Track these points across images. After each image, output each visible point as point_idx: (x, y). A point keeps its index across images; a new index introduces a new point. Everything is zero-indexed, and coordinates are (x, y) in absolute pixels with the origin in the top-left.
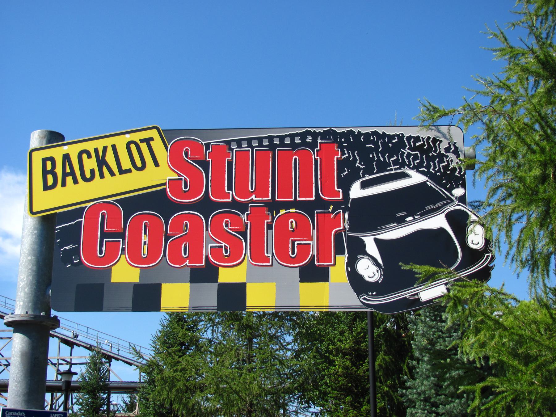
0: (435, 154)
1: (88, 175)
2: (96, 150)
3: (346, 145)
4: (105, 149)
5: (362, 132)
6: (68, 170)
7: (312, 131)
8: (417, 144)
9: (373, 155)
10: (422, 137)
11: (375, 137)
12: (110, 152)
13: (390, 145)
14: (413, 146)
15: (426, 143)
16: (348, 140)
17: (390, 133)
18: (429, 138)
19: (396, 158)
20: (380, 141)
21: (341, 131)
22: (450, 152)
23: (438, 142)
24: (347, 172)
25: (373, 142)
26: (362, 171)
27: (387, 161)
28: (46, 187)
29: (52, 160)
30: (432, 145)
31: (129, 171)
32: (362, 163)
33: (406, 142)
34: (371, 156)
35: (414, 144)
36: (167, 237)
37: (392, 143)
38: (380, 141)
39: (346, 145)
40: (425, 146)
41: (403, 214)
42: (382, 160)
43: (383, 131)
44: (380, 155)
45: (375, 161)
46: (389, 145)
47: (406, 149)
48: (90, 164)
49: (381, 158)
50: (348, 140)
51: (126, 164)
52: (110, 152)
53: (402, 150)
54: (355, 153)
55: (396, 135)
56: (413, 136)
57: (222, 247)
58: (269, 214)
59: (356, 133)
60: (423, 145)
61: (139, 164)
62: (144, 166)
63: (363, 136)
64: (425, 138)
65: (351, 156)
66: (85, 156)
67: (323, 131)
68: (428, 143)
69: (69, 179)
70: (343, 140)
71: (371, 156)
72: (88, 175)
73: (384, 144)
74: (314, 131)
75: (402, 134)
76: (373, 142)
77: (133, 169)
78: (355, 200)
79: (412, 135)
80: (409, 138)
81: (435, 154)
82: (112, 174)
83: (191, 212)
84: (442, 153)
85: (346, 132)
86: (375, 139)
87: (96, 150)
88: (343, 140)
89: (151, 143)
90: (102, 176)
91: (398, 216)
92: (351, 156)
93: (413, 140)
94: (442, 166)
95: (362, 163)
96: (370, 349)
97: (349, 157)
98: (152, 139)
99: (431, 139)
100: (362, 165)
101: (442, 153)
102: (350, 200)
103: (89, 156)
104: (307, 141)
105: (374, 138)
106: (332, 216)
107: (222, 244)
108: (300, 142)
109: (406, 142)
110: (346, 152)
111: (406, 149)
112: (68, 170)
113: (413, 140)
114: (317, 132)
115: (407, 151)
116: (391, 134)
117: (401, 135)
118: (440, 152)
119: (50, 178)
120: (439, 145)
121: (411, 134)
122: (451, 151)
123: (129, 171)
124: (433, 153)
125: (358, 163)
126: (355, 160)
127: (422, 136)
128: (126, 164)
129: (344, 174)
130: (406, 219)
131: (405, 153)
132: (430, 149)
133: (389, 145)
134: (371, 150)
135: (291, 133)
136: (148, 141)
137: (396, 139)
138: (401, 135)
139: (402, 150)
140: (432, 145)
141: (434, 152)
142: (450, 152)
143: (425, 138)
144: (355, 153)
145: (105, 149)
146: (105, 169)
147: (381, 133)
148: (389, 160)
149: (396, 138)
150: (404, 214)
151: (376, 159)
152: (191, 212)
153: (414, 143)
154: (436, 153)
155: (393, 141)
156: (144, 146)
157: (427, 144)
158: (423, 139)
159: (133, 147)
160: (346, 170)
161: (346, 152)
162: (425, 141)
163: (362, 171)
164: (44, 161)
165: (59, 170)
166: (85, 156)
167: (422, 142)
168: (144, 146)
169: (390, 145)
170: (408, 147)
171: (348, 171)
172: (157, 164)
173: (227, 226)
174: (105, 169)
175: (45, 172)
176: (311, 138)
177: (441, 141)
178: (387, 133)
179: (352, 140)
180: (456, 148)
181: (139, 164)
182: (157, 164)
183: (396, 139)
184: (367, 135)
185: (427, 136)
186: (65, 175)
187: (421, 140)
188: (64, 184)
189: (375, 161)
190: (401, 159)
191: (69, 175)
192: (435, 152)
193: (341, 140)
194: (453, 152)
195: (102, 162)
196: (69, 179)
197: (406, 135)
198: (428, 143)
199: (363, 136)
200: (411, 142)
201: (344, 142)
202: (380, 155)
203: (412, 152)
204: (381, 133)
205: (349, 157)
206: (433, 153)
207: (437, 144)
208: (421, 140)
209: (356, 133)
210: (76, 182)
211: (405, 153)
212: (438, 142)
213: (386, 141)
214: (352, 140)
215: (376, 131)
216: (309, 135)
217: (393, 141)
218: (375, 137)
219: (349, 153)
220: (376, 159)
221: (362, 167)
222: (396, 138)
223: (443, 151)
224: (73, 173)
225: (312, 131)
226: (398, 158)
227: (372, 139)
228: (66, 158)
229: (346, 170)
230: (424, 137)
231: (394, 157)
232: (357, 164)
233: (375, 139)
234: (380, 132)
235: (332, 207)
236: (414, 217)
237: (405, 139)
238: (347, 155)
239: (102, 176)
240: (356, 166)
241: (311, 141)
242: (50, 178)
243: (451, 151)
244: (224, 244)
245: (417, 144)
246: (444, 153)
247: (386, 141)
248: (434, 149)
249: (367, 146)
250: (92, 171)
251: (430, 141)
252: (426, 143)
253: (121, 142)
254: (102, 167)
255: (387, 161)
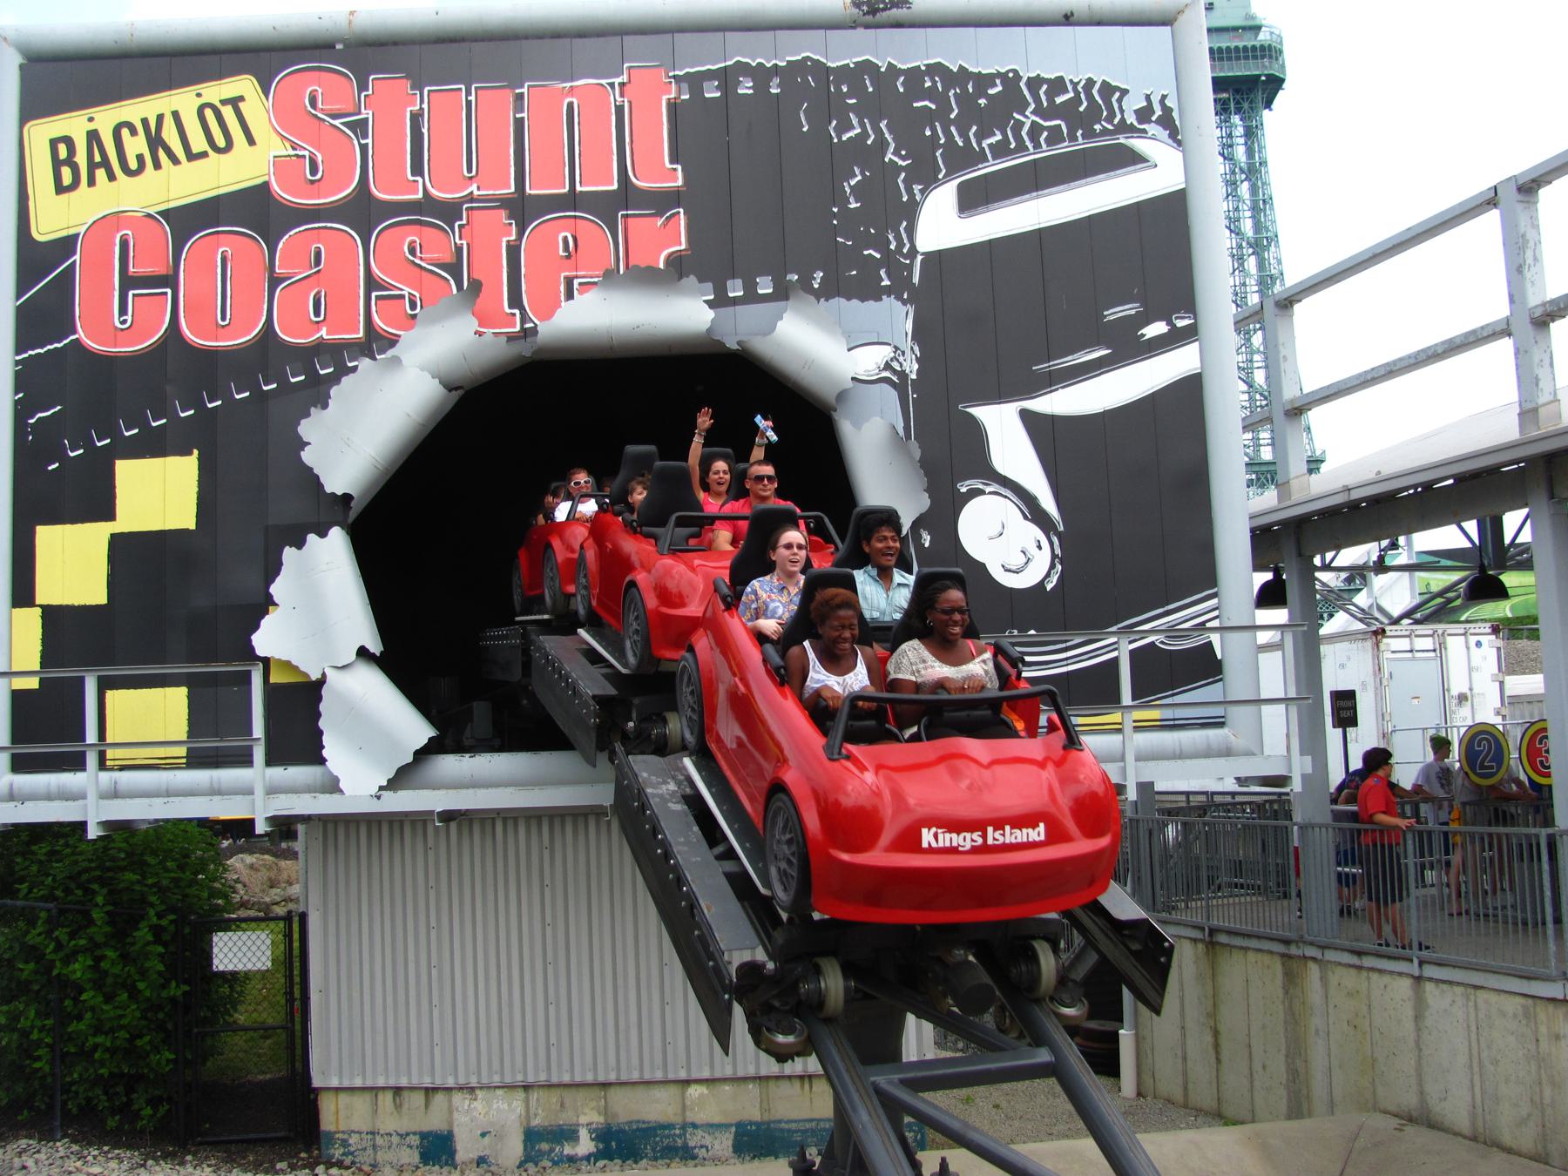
0: (1110, 127)
1: (133, 165)
2: (145, 122)
3: (854, 101)
4: (160, 118)
5: (899, 66)
6: (98, 158)
7: (754, 64)
8: (1059, 100)
9: (934, 130)
10: (1071, 81)
11: (937, 79)
12: (169, 123)
13: (982, 102)
14: (1045, 104)
15: (1083, 96)
16: (857, 90)
17: (980, 69)
18: (1090, 83)
19: (999, 137)
20: (953, 91)
21: (910, 66)
22: (1150, 121)
23: (1117, 95)
24: (859, 178)
25: (930, 94)
26: (903, 175)
27: (975, 145)
28: (60, 189)
29: (69, 141)
30: (1100, 102)
31: (204, 155)
32: (903, 153)
33: (1026, 92)
34: (928, 133)
35: (1051, 100)
36: (275, 282)
37: (988, 97)
38: (953, 91)
39: (854, 101)
40: (1081, 103)
41: (1128, 310)
42: (961, 144)
43: (960, 62)
44: (953, 129)
45: (941, 146)
46: (980, 101)
47: (1027, 113)
48: (136, 146)
49: (957, 138)
50: (857, 90)
51: (198, 143)
52: (169, 123)
53: (1015, 115)
54: (883, 125)
55: (999, 75)
56: (1046, 76)
57: (403, 297)
58: (511, 224)
59: (883, 70)
60: (1077, 100)
61: (221, 143)
62: (230, 145)
63: (902, 79)
64: (1078, 83)
65: (870, 132)
66: (125, 132)
67: (785, 64)
68: (1090, 97)
69: (101, 174)
70: (845, 89)
71: (928, 133)
72: (133, 165)
73: (965, 100)
74: (759, 64)
75: (1015, 72)
76: (930, 94)
77: (210, 152)
78: (936, 259)
79: (1042, 75)
80: (1033, 84)
81: (1110, 127)
82: (176, 161)
83: (329, 225)
84: (1129, 122)
85: (852, 66)
86: (939, 85)
87: (145, 122)
88: (845, 89)
89: (241, 105)
90: (157, 166)
91: (1112, 318)
92: (870, 132)
93: (1045, 87)
94: (990, 146)
95: (903, 153)
96: (1014, 692)
97: (864, 134)
98: (241, 98)
99: (1097, 86)
100: (903, 158)
101: (1129, 122)
102: (919, 258)
103: (134, 132)
104: (740, 91)
105: (934, 82)
106: (659, 224)
107: (402, 290)
108: (718, 94)
109: (1026, 92)
110: (855, 121)
111: (1027, 113)
112: (98, 158)
113: (1045, 87)
114: (768, 65)
115: (1029, 118)
116: (984, 72)
117: (1011, 75)
118: (1123, 119)
119: (67, 174)
120: (1120, 101)
121: (1038, 72)
122: (1154, 118)
123: (204, 155)
124: (1103, 123)
125: (893, 154)
126: (882, 144)
127: (1070, 77)
128: (198, 143)
129: (853, 183)
130: (1143, 331)
131: (1023, 123)
132: (1094, 112)
133: (980, 101)
134: (928, 117)
135: (692, 70)
136: (235, 102)
137: (996, 85)
138: (1011, 75)
139: (1015, 115)
140: (1100, 102)
141: (1105, 120)
142: (1152, 121)
143: (1078, 83)
144: (883, 125)
145: (160, 118)
146: (162, 154)
147: (955, 70)
148: (979, 144)
149: (998, 81)
150: (1133, 312)
151: (942, 141)
152: (329, 225)
153: (1051, 95)
154: (1113, 125)
155: (991, 92)
156: (228, 112)
157: (1086, 99)
158: (1075, 85)
159: (209, 113)
160: (857, 170)
161: (855, 121)
162: (1080, 90)
163: (903, 175)
164: (54, 143)
165: (81, 159)
166: (125, 132)
167: (1071, 95)
168: (228, 112)
169: (982, 102)
170: (1033, 106)
171: (862, 173)
172: (251, 141)
173: (412, 251)
174: (162, 154)
175: (57, 164)
176: (751, 84)
177: (1124, 92)
178: (971, 69)
179: (870, 90)
180: (1167, 111)
181: (221, 143)
182: (251, 141)
183: (996, 85)
184: (914, 75)
185: (1086, 77)
186: (92, 166)
187: (1070, 88)
188: (92, 182)
189: (941, 146)
190: (1015, 141)
191: (99, 165)
192: (1110, 119)
193: (838, 89)
194: (1159, 122)
195: (155, 141)
196: (101, 174)
197: (1025, 75)
198: (1090, 97)
199: (902, 79)
200: (1042, 92)
201: (849, 95)
202: (953, 129)
203: (1045, 120)
204: (955, 70)
205: (864, 134)
206: (1103, 123)
207: (1114, 100)
208: (1070, 88)
209: (883, 70)
210: (112, 177)
211: (1023, 123)
212: (1117, 95)
213: (971, 90)
214: (870, 90)
215: (939, 62)
216: (743, 77)
217: (991, 92)
218: (937, 79)
219: (862, 125)
220: (942, 141)
221: (904, 164)
222: (998, 81)
223: (1131, 119)
224: (105, 163)
225: (754, 64)
226: (1006, 139)
227: (928, 84)
228: (93, 136)
229: (857, 170)
230: (1076, 80)
231: (995, 135)
232: (889, 156)
233: (939, 85)
234: (951, 67)
235: (821, 274)
236: (1170, 323)
237: (1022, 85)
238: (858, 130)
239: (157, 166)
240: (887, 160)
241: (751, 92)
242: (67, 174)
243: (1154, 118)
244: (406, 291)
245: (1059, 100)
246: (1135, 123)
247: (971, 90)
248: (1105, 113)
249: (915, 105)
250: (140, 158)
251: (1095, 92)
252: (1083, 96)
253: (525, 115)
254: (157, 150)
255: (975, 145)
